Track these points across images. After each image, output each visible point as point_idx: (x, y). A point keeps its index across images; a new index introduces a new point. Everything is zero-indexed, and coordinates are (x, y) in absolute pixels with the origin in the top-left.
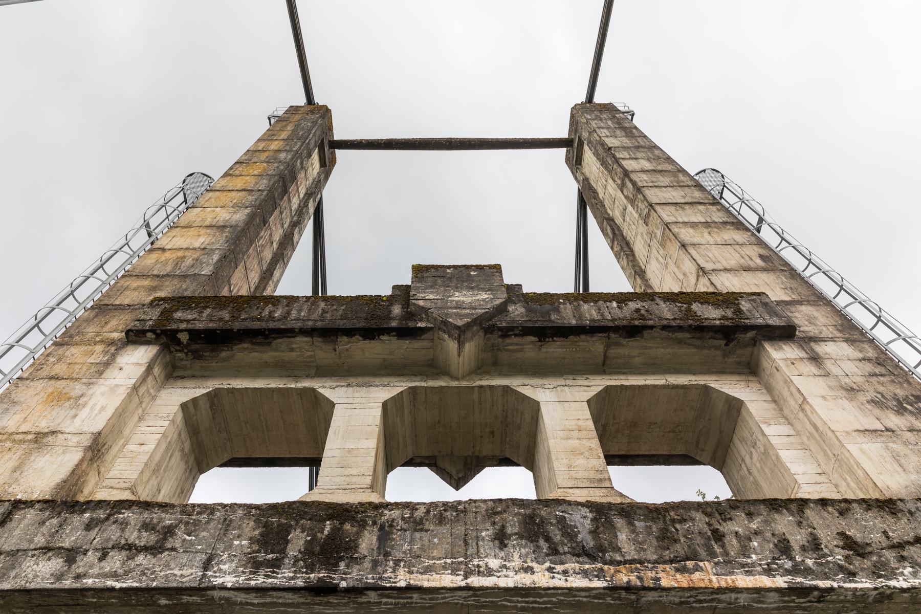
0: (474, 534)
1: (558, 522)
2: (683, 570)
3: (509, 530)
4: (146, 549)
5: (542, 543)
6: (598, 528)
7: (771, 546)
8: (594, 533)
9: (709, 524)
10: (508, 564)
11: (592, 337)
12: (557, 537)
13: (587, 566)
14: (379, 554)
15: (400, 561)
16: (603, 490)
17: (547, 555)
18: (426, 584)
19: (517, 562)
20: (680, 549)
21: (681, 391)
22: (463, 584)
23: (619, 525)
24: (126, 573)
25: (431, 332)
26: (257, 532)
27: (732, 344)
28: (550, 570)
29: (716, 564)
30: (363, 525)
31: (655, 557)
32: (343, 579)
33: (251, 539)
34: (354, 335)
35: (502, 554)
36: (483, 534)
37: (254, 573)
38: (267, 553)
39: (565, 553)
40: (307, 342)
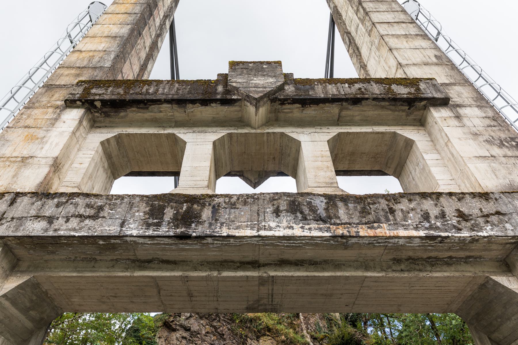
0: (263, 210)
1: (308, 204)
2: (372, 228)
3: (281, 208)
4: (89, 217)
5: (298, 214)
6: (328, 207)
7: (420, 216)
8: (326, 209)
9: (388, 205)
10: (280, 225)
11: (332, 104)
12: (306, 211)
13: (321, 226)
14: (213, 220)
15: (224, 223)
16: (333, 188)
17: (301, 220)
18: (237, 235)
19: (285, 224)
20: (371, 217)
21: (380, 135)
22: (256, 234)
23: (340, 206)
24: (80, 229)
25: (240, 102)
26: (147, 209)
27: (412, 109)
28: (302, 228)
29: (389, 225)
30: (203, 206)
31: (358, 221)
32: (194, 232)
33: (144, 212)
34: (196, 103)
35: (277, 220)
36: (268, 210)
37: (147, 229)
38: (153, 219)
39: (310, 220)
40: (169, 107)
